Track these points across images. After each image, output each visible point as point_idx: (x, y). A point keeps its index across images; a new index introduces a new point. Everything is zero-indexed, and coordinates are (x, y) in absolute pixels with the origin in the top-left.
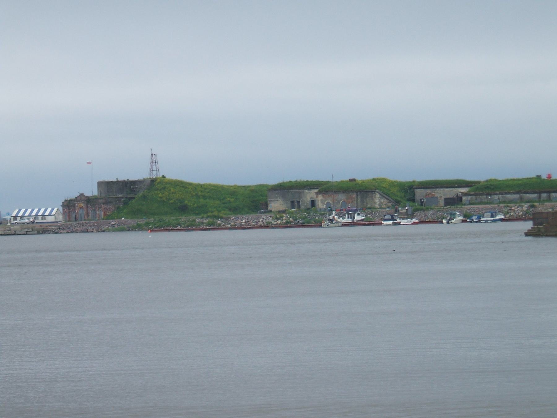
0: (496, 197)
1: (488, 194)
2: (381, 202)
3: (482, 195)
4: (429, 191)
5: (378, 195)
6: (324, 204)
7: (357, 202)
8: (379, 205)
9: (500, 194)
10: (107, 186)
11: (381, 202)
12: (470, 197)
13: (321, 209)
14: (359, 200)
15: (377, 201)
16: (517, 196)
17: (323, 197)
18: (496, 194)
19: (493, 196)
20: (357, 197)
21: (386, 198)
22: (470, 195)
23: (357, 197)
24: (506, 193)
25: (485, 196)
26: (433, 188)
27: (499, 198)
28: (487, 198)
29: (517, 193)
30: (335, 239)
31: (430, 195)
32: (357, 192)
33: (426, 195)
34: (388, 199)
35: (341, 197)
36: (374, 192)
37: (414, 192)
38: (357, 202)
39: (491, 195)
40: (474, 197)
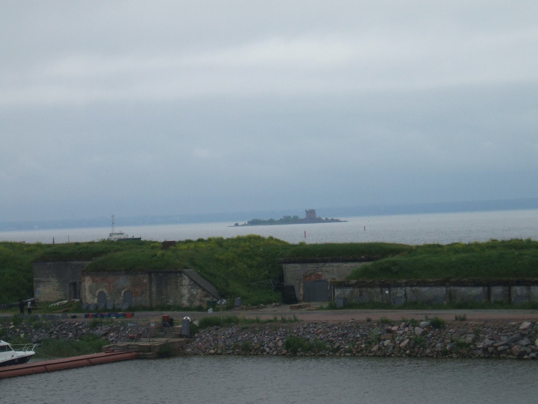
0: (400, 292)
1: (384, 285)
2: (192, 295)
3: (372, 285)
4: (310, 267)
5: (186, 281)
6: (94, 295)
7: (151, 294)
8: (189, 300)
9: (407, 285)
10: (310, 210)
11: (192, 295)
12: (348, 291)
13: (88, 306)
14: (154, 289)
15: (185, 291)
16: (441, 291)
17: (93, 281)
18: (400, 285)
19: (394, 290)
20: (150, 283)
21: (200, 286)
22: (349, 286)
23: (150, 283)
24: (424, 284)
25: (378, 290)
26: (317, 262)
27: (405, 295)
28: (382, 292)
29: (442, 284)
30: (105, 367)
31: (313, 277)
32: (150, 273)
33: (305, 276)
34: (204, 290)
35: (124, 282)
36: (181, 272)
37: (281, 268)
38: (151, 294)
39: (388, 286)
40: (357, 291)
